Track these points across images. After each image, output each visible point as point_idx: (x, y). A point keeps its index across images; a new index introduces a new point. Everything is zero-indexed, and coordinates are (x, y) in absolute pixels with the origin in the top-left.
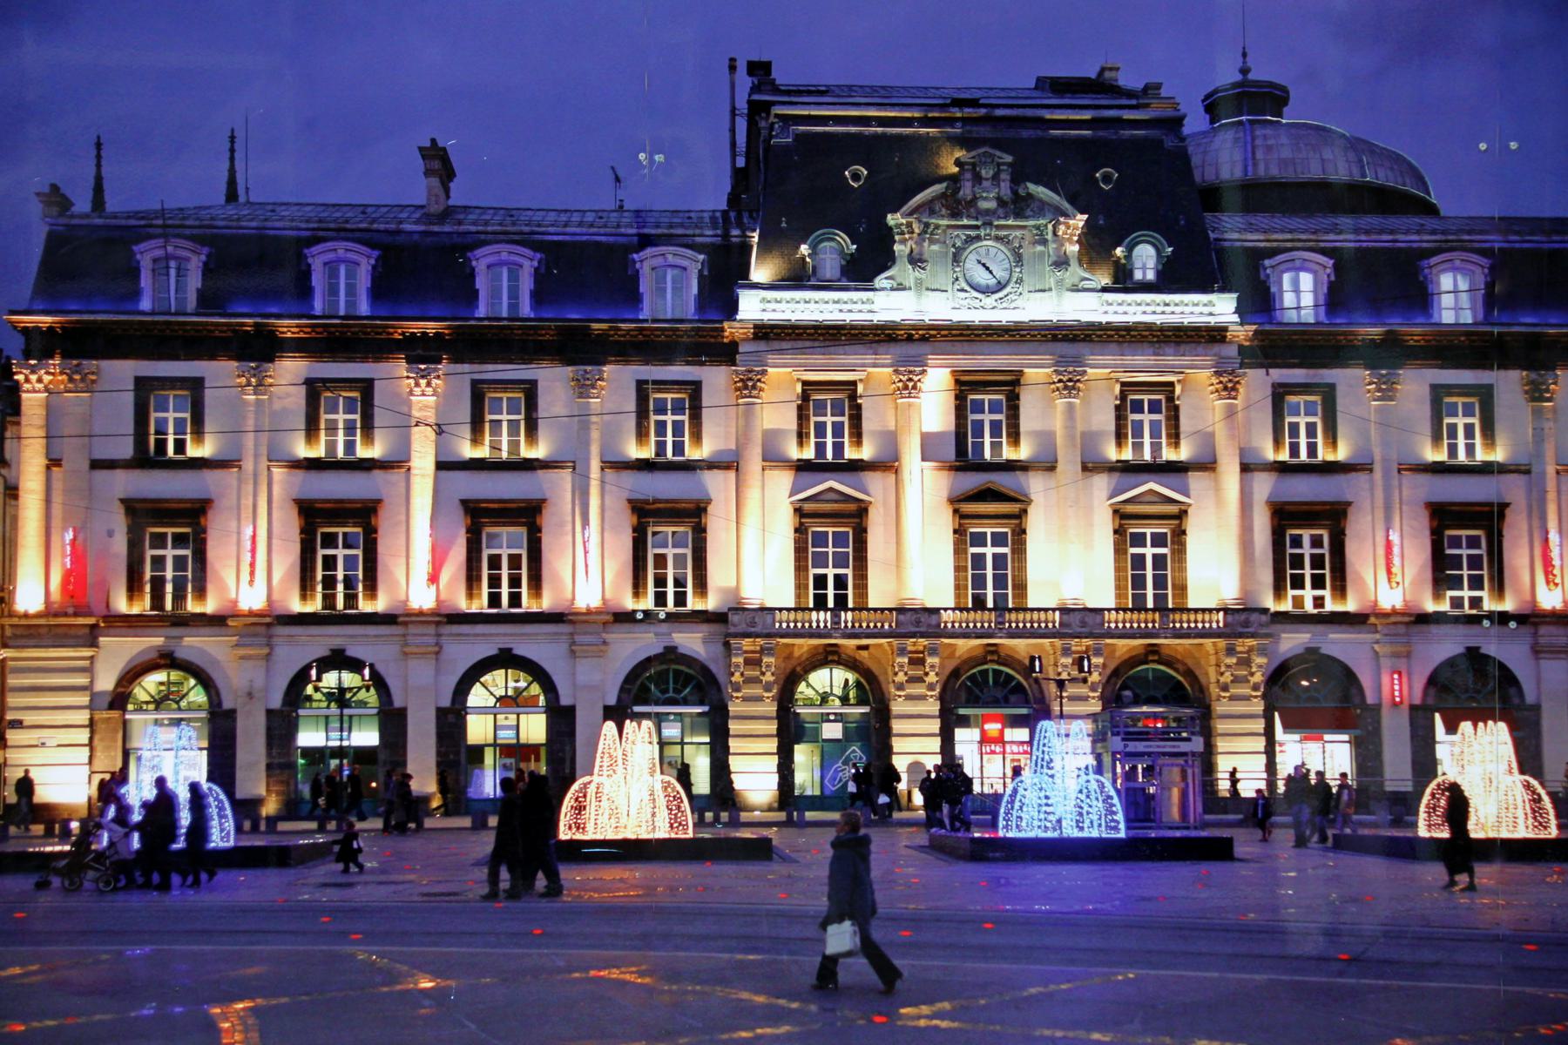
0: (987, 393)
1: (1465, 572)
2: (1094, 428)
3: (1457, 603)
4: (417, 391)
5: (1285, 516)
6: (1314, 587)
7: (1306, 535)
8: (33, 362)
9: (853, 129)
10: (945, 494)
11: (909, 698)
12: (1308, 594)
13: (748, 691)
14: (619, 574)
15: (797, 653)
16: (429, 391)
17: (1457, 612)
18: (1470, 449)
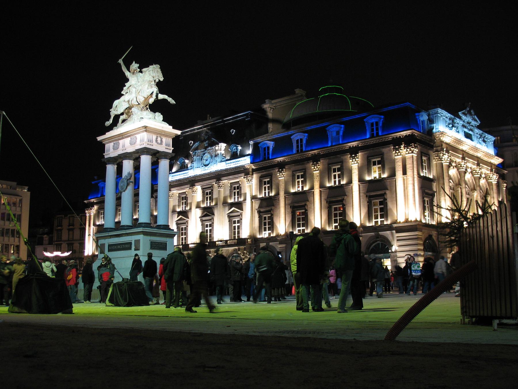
12: (379, 220)
16: (356, 162)
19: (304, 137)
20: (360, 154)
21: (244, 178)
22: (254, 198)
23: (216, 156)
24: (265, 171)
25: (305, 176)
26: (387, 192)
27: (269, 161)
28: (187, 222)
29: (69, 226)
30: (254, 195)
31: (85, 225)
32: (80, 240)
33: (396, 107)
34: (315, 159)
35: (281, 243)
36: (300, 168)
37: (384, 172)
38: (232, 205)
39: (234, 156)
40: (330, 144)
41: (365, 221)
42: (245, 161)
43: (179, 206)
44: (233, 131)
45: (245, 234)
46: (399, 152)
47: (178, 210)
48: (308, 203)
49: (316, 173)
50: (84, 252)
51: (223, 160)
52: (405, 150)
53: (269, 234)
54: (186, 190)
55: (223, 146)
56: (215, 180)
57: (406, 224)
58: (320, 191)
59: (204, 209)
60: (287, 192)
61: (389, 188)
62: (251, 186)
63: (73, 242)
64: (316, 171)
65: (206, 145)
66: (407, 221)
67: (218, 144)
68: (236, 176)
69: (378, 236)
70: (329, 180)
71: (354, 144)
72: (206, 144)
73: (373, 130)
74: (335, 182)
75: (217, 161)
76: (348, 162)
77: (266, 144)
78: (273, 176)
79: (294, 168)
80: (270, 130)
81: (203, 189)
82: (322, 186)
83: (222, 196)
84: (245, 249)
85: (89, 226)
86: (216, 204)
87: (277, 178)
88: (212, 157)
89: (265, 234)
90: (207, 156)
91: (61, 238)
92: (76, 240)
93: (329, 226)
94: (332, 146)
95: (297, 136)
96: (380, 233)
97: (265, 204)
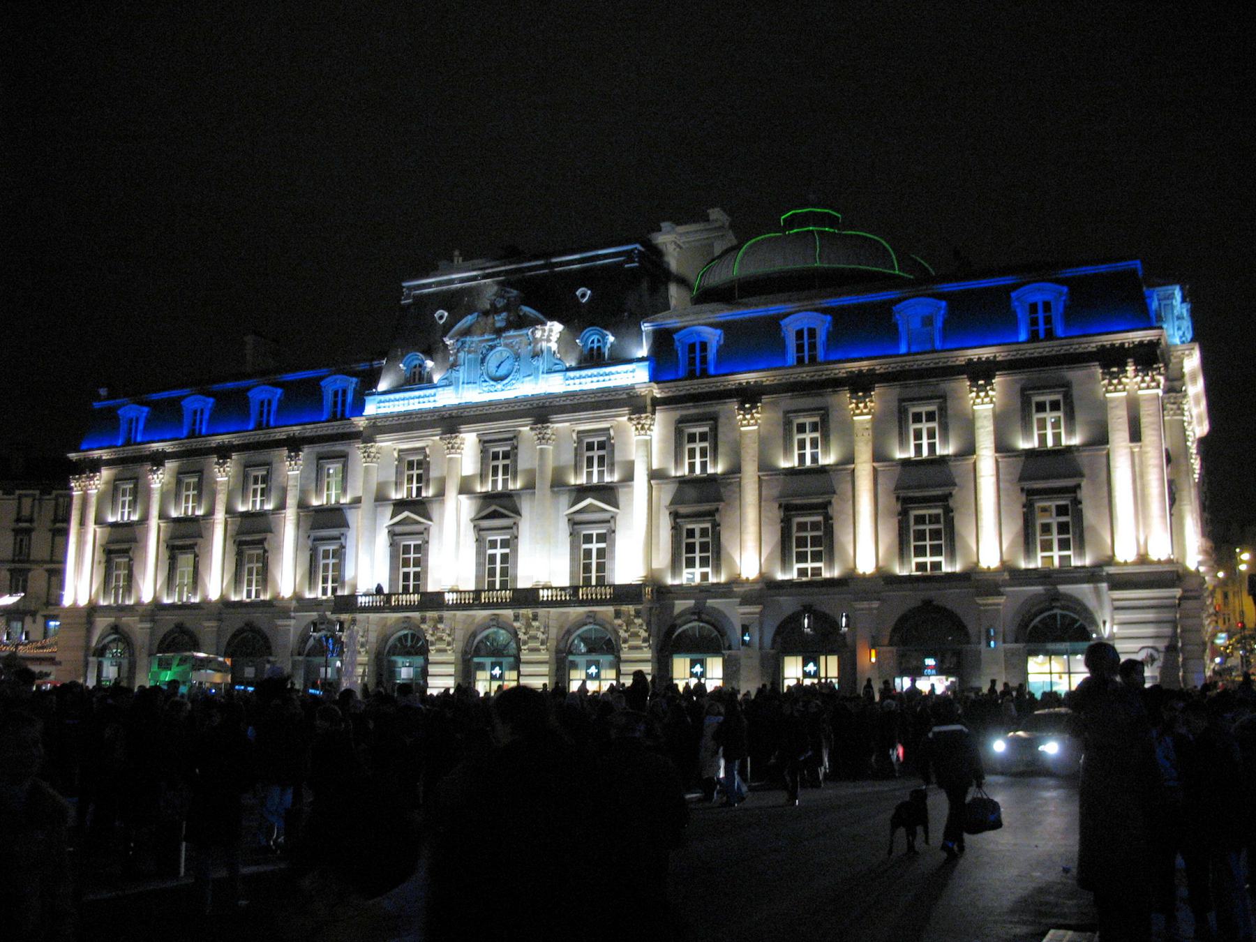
2: (562, 464)
3: (802, 572)
4: (978, 401)
5: (789, 510)
6: (1061, 549)
9: (444, 288)
10: (892, 487)
12: (1056, 554)
13: (532, 644)
14: (302, 577)
15: (389, 623)
16: (987, 400)
19: (822, 325)
20: (235, 456)
21: (630, 419)
22: (654, 475)
23: (536, 355)
24: (695, 407)
26: (1084, 483)
27: (706, 380)
28: (427, 529)
29: (18, 520)
30: (655, 467)
31: (67, 520)
32: (52, 561)
33: (1102, 269)
34: (860, 385)
35: (746, 600)
36: (810, 400)
37: (945, 440)
38: (582, 492)
39: (593, 359)
40: (903, 349)
42: (635, 376)
43: (398, 485)
44: (584, 294)
45: (627, 568)
46: (1120, 383)
47: (395, 495)
49: (863, 420)
50: (61, 596)
51: (557, 368)
52: (1139, 379)
53: (705, 576)
54: (431, 441)
55: (556, 327)
56: (529, 420)
57: (1145, 569)
58: (875, 470)
59: (487, 498)
60: (766, 467)
61: (1086, 471)
62: (646, 444)
63: (27, 566)
64: (984, 405)
65: (498, 325)
66: (1143, 559)
67: (543, 324)
68: (603, 413)
69: (1055, 597)
70: (787, 451)
71: (985, 353)
72: (500, 320)
73: (1034, 322)
74: (692, 466)
75: (538, 368)
76: (212, 471)
77: (699, 334)
78: (722, 420)
79: (787, 401)
80: (673, 302)
81: (484, 443)
83: (550, 464)
84: (638, 614)
85: (82, 523)
86: (530, 487)
87: (735, 428)
88: (517, 357)
89: (691, 576)
90: (501, 352)
91: (29, 555)
92: (36, 562)
94: (908, 354)
95: (800, 318)
96: (1063, 588)
97: (691, 493)
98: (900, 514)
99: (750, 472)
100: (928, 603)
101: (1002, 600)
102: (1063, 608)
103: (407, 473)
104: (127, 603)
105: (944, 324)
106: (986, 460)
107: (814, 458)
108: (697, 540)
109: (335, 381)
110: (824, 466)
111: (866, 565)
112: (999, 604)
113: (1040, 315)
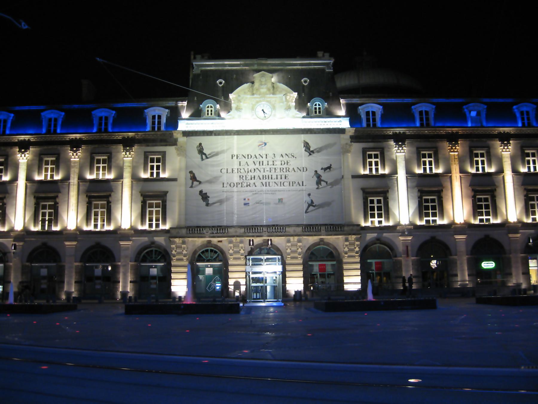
0: (101, 156)
1: (484, 210)
3: (428, 221)
7: (375, 199)
8: (23, 150)
9: (220, 68)
11: (235, 259)
12: (376, 220)
14: (137, 218)
16: (402, 151)
17: (427, 225)
18: (377, 170)
19: (377, 109)
25: (383, 156)
37: (437, 166)
41: (136, 222)
48: (60, 195)
64: (506, 153)
70: (39, 173)
71: (507, 130)
82: (29, 179)
93: (35, 226)
98: (473, 197)
99: (74, 180)
100: (487, 237)
101: (519, 235)
102: (155, 247)
103: (150, 164)
104: (54, 229)
105: (113, 121)
106: (509, 176)
107: (52, 176)
108: (376, 205)
109: (154, 110)
110: (55, 180)
111: (126, 225)
112: (517, 237)
113: (525, 117)
